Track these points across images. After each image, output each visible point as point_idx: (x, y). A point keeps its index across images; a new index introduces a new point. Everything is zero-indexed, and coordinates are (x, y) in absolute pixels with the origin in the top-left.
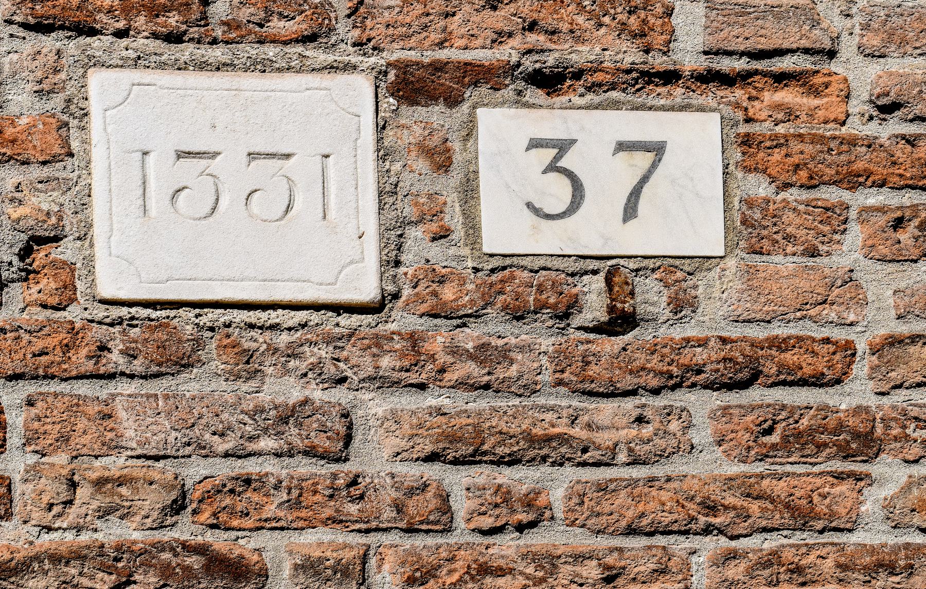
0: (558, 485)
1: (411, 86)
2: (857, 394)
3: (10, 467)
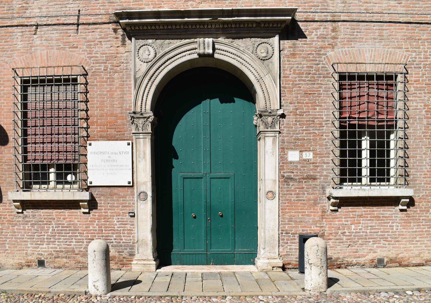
0: (306, 168)
1: (301, 151)
2: (318, 164)
3: (9, 193)
